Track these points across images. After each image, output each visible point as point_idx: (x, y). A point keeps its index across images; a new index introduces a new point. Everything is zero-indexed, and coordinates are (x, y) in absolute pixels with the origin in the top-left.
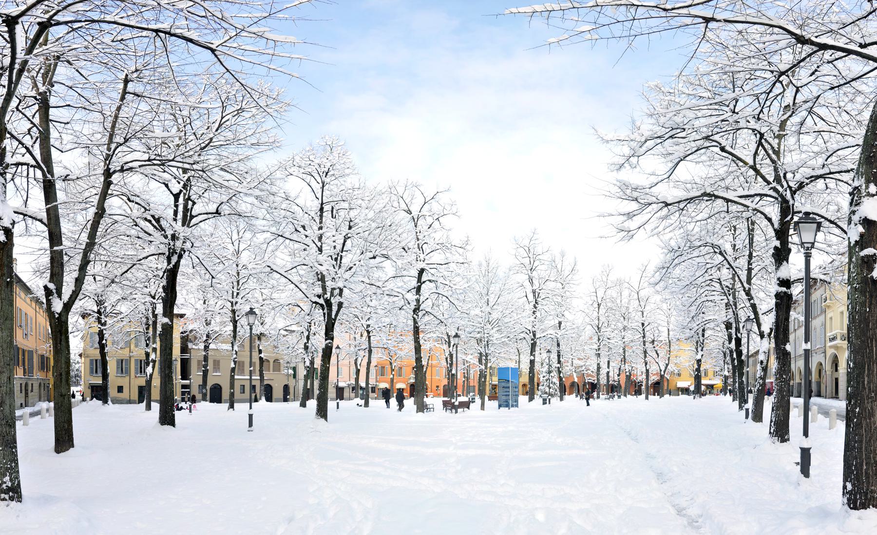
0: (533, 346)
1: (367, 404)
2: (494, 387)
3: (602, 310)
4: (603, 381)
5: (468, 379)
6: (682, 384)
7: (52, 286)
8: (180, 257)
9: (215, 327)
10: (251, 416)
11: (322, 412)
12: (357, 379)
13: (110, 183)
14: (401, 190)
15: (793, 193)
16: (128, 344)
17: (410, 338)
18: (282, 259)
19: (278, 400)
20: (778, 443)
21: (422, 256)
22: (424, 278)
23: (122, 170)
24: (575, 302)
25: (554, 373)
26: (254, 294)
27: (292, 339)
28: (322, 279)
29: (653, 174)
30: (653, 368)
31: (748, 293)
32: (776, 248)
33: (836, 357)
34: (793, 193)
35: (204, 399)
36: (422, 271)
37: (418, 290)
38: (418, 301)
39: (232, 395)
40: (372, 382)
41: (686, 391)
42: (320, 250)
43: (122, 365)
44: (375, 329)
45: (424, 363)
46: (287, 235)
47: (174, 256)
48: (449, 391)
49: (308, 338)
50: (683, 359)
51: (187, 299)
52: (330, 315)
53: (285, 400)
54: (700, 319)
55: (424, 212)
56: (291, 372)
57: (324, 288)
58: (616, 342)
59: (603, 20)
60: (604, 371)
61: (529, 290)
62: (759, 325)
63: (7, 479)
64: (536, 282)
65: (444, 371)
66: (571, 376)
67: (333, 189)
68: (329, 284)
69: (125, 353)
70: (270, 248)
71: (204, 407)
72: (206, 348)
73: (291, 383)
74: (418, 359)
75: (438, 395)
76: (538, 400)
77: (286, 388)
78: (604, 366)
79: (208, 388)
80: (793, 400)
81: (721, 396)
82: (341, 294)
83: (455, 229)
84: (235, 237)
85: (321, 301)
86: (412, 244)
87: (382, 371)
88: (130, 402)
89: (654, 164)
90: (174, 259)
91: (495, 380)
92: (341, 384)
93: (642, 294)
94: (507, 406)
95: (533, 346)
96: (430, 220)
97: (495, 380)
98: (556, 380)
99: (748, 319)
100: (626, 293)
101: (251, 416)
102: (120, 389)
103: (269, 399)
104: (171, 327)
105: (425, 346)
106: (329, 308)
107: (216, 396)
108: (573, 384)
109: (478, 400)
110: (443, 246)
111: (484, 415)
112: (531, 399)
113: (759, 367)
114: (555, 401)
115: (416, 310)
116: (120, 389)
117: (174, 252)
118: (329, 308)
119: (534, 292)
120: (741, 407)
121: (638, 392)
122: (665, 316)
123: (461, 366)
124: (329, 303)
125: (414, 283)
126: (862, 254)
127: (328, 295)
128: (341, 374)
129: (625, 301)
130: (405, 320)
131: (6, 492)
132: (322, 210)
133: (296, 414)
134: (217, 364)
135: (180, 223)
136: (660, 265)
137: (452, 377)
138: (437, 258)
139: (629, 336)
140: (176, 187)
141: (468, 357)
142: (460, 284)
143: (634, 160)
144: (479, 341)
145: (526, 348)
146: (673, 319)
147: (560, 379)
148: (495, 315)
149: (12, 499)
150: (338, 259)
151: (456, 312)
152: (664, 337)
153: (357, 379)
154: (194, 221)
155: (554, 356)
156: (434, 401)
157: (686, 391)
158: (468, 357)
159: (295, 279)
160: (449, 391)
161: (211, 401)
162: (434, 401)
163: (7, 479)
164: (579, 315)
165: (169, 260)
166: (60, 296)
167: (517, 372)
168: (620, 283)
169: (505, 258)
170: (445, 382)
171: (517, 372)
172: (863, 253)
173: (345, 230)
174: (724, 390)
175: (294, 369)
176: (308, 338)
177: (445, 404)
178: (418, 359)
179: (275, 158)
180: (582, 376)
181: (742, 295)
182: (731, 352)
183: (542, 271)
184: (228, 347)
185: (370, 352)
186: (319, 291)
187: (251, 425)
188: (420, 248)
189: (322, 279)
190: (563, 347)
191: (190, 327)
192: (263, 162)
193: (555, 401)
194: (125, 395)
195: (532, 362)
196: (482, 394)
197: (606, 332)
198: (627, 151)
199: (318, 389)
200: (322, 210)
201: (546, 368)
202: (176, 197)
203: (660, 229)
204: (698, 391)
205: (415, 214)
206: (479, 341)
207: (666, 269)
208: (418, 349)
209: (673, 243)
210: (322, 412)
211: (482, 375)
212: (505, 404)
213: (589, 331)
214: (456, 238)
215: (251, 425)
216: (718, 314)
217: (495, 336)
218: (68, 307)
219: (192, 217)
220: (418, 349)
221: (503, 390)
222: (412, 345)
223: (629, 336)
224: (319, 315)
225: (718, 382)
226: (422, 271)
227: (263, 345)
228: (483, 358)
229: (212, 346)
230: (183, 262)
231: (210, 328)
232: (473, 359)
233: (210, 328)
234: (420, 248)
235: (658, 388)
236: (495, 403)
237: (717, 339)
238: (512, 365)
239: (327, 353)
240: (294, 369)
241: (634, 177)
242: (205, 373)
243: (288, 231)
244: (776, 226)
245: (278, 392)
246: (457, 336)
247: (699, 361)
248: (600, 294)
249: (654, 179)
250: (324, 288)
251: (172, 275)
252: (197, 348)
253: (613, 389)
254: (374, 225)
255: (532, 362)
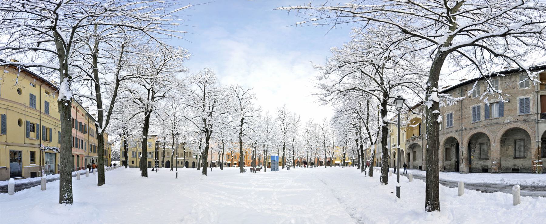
0: (284, 148)
1: (222, 169)
2: (269, 163)
3: (309, 135)
4: (309, 161)
5: (260, 160)
6: (337, 162)
7: (98, 124)
8: (150, 112)
9: (167, 140)
10: (177, 173)
11: (205, 172)
12: (219, 160)
13: (119, 84)
14: (235, 88)
15: (390, 88)
16: (136, 146)
17: (238, 145)
18: (191, 114)
19: (190, 167)
20: (384, 185)
21: (243, 113)
22: (244, 121)
23: (123, 79)
24: (299, 132)
25: (292, 158)
26: (181, 128)
27: (195, 145)
28: (204, 120)
29: (334, 81)
30: (328, 156)
31: (367, 129)
32: (382, 110)
33: (395, 152)
34: (390, 88)
35: (163, 167)
36: (243, 119)
37: (241, 126)
38: (241, 129)
39: (172, 165)
40: (224, 161)
41: (338, 165)
42: (204, 110)
43: (134, 154)
44: (225, 140)
45: (244, 154)
46: (192, 105)
47: (148, 112)
48: (253, 164)
49: (201, 144)
50: (338, 153)
51: (153, 129)
52: (208, 135)
53: (193, 167)
54: (346, 138)
55: (244, 97)
56: (195, 157)
57: (205, 124)
58: (314, 146)
59: (323, 16)
60: (309, 158)
61: (283, 127)
62: (371, 140)
63: (66, 195)
64: (285, 124)
65: (251, 157)
66: (297, 159)
67: (209, 87)
68: (207, 123)
69: (135, 150)
70: (185, 110)
71: (164, 171)
72: (164, 147)
73: (196, 161)
74: (241, 152)
75: (249, 166)
76: (286, 168)
77: (194, 163)
78: (309, 156)
79: (165, 162)
80: (390, 169)
81: (352, 167)
82: (212, 128)
83: (255, 104)
84: (174, 106)
85: (205, 130)
86: (239, 109)
87: (228, 157)
88: (136, 167)
89: (335, 76)
90: (148, 113)
91: (270, 161)
92: (213, 161)
93: (324, 129)
94: (275, 170)
95: (284, 148)
96: (246, 100)
97: (270, 161)
98: (292, 161)
99: (366, 138)
100: (317, 129)
101: (177, 173)
102: (133, 162)
103: (187, 167)
104: (147, 139)
105: (244, 148)
106: (207, 132)
107: (168, 165)
108: (298, 162)
109: (263, 168)
110: (251, 110)
111: (265, 173)
112: (283, 168)
113: (371, 156)
114: (292, 168)
115: (241, 133)
116: (133, 162)
117: (148, 111)
118: (207, 132)
119: (284, 128)
120: (362, 171)
121: (321, 165)
122: (333, 138)
123: (257, 155)
124: (207, 130)
125: (240, 123)
126: (433, 112)
127: (207, 127)
128: (212, 158)
129: (317, 131)
130: (236, 138)
131: (66, 200)
132: (204, 95)
133: (196, 172)
134: (168, 154)
135: (150, 100)
136: (334, 117)
137: (254, 159)
138: (249, 114)
139: (318, 144)
140: (148, 87)
141: (260, 152)
142: (257, 124)
143: (327, 76)
144: (264, 146)
145: (281, 149)
146: (335, 138)
147: (294, 160)
148: (270, 136)
149: (68, 203)
150: (210, 115)
151: (255, 134)
152: (331, 146)
153: (219, 160)
154: (155, 99)
155: (292, 152)
156: (247, 168)
157: (338, 165)
158: (260, 152)
159: (196, 122)
160: (253, 164)
161: (166, 167)
162: (247, 168)
163: (66, 195)
164: (301, 137)
165: (146, 113)
166: (101, 127)
167: (278, 157)
168: (315, 125)
169: (274, 115)
170: (251, 161)
171: (278, 157)
172: (433, 112)
173: (213, 102)
174: (353, 165)
175: (197, 156)
176: (201, 144)
177: (251, 169)
178: (241, 152)
179: (187, 74)
180: (301, 159)
181: (364, 129)
182: (358, 150)
183: (287, 120)
184: (171, 147)
185: (224, 149)
186: (204, 126)
187: (177, 177)
188: (242, 110)
189: (204, 120)
190: (295, 149)
191: (159, 140)
192: (180, 76)
193: (292, 168)
194: (135, 165)
195: (284, 154)
196: (265, 166)
197: (311, 143)
198: (324, 71)
199: (204, 164)
200: (204, 95)
201: (288, 156)
202: (149, 90)
203: (336, 102)
204: (345, 164)
205: (240, 97)
206: (264, 146)
207: (335, 118)
208: (241, 148)
209: (339, 108)
210: (205, 172)
211: (265, 159)
212: (273, 169)
213: (304, 143)
214: (256, 107)
215: (177, 177)
216: (352, 136)
217: (270, 144)
218: (103, 131)
219: (154, 98)
220: (241, 148)
221: (273, 164)
222: (239, 148)
223: (318, 144)
224: (204, 136)
225: (350, 162)
226: (243, 119)
227: (185, 147)
228: (265, 152)
229: (166, 147)
230: (151, 114)
231: (165, 140)
232: (262, 153)
233: (165, 140)
234: (242, 110)
235: (329, 163)
236: (270, 169)
237: (352, 144)
238: (276, 155)
239: (207, 149)
240: (197, 156)
241: (327, 82)
242: (164, 157)
243: (192, 103)
244: (382, 101)
245: (190, 164)
246: (256, 143)
247: (345, 154)
248: (309, 129)
249: (334, 83)
250: (205, 124)
251: (147, 119)
252: (161, 147)
253: (312, 164)
254: (224, 101)
255: (284, 154)
